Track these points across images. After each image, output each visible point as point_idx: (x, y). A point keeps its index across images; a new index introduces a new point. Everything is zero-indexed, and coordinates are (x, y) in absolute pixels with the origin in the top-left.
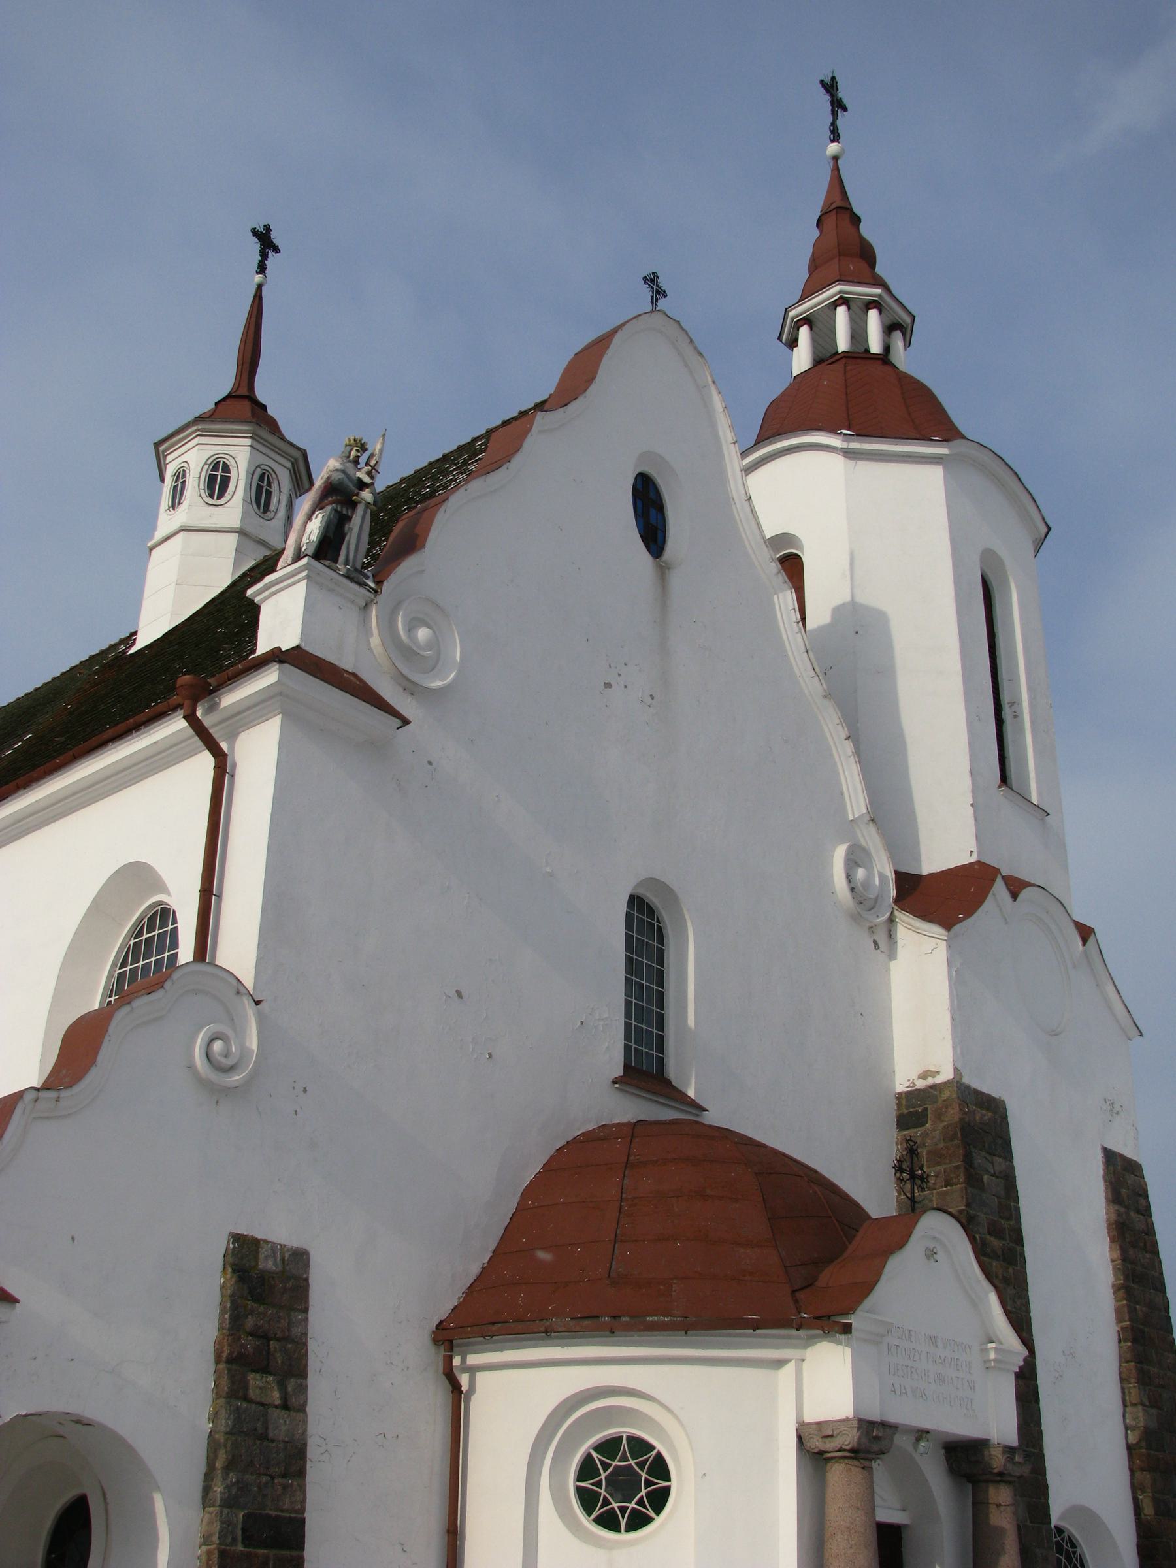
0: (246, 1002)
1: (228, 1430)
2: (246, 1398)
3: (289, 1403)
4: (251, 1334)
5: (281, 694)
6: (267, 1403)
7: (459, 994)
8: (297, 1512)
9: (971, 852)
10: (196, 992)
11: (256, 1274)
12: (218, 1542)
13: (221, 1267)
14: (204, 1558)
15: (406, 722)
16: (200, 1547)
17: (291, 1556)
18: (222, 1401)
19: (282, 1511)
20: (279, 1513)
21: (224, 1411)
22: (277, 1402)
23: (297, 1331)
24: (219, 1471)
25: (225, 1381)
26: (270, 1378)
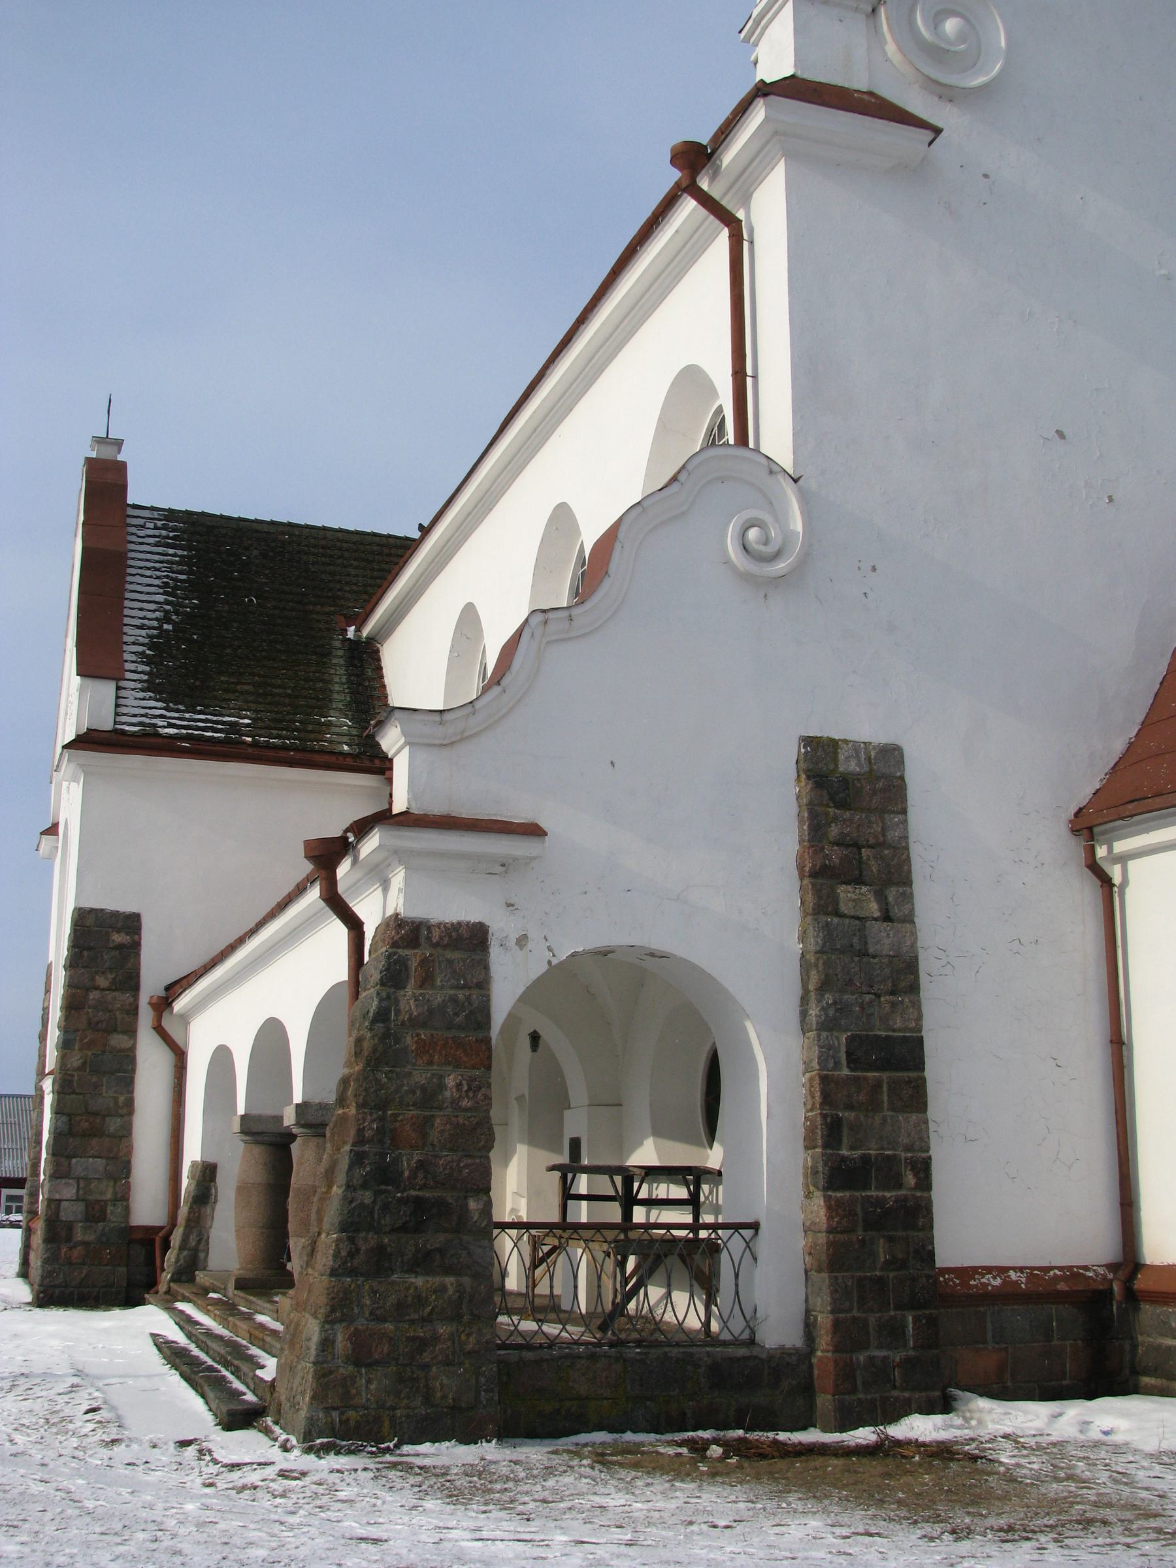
0: (782, 480)
1: (818, 948)
2: (837, 913)
3: (890, 914)
4: (837, 844)
5: (776, 133)
6: (864, 916)
7: (1061, 434)
8: (911, 1030)
10: (722, 480)
11: (836, 777)
12: (818, 1067)
13: (794, 775)
14: (808, 1085)
15: (937, 131)
16: (804, 1074)
17: (909, 1077)
18: (809, 919)
19: (894, 1031)
20: (891, 1034)
21: (811, 929)
22: (877, 914)
23: (893, 835)
24: (812, 994)
25: (809, 897)
26: (865, 889)
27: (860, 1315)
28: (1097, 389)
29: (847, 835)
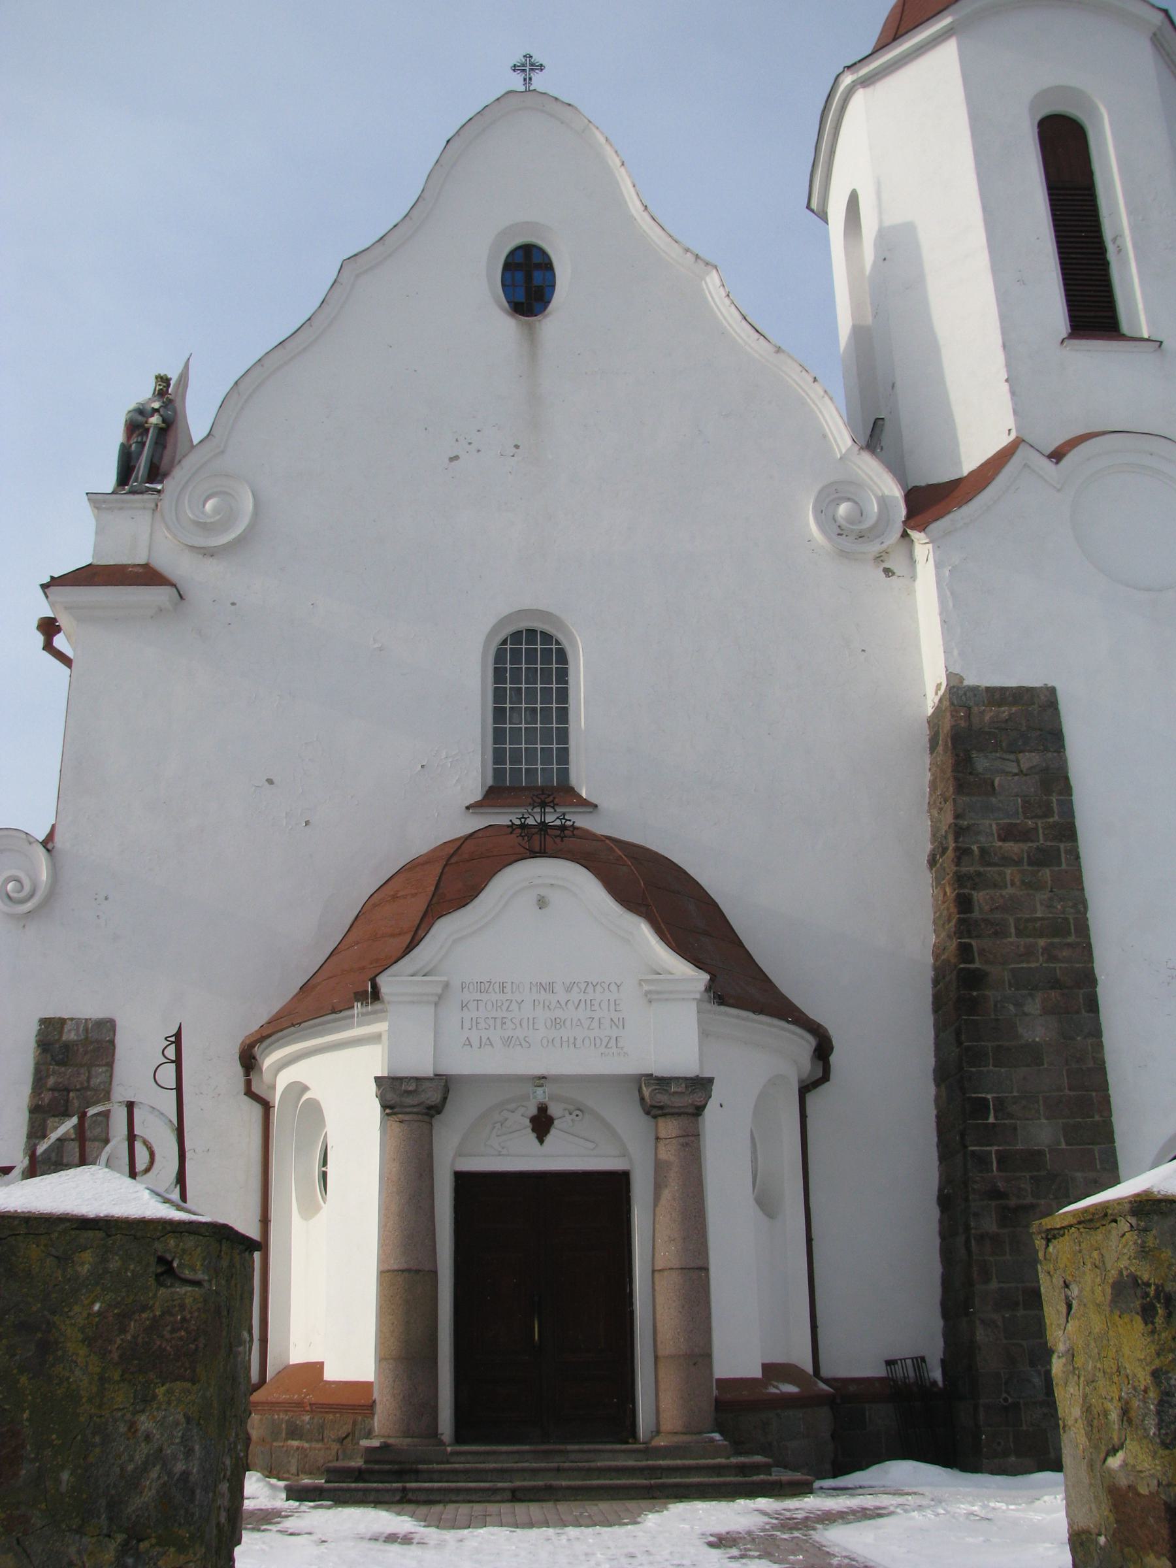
9: (1010, 430)
27: (1049, 844)
28: (306, 743)
29: (60, 1083)
